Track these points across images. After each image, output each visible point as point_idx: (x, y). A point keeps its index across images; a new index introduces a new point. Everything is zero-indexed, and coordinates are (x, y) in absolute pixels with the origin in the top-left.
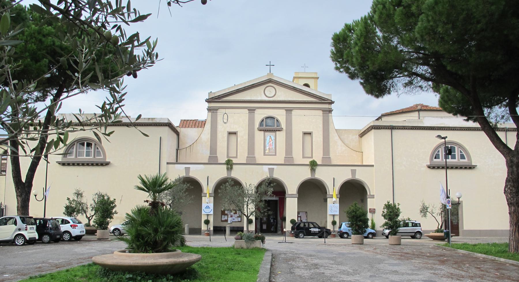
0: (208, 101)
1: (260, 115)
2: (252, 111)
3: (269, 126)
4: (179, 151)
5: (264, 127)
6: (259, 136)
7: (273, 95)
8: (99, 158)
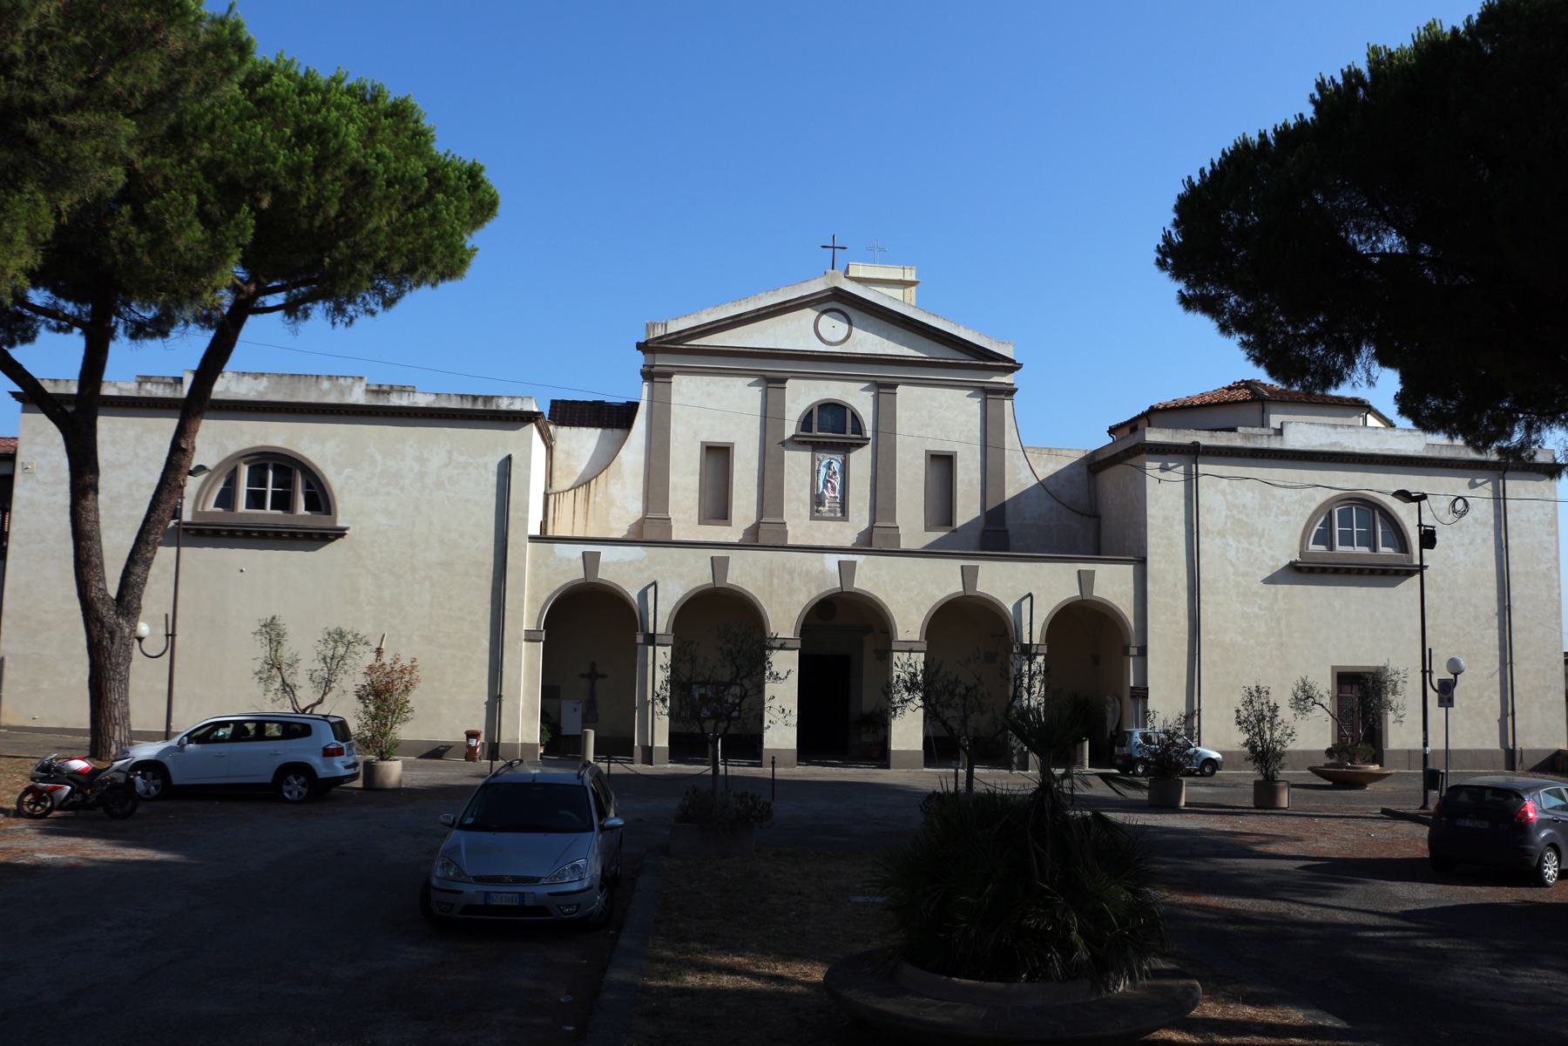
0: (643, 347)
1: (801, 396)
2: (773, 384)
3: (831, 430)
4: (552, 499)
5: (849, 434)
6: (797, 463)
7: (841, 338)
8: (319, 521)
